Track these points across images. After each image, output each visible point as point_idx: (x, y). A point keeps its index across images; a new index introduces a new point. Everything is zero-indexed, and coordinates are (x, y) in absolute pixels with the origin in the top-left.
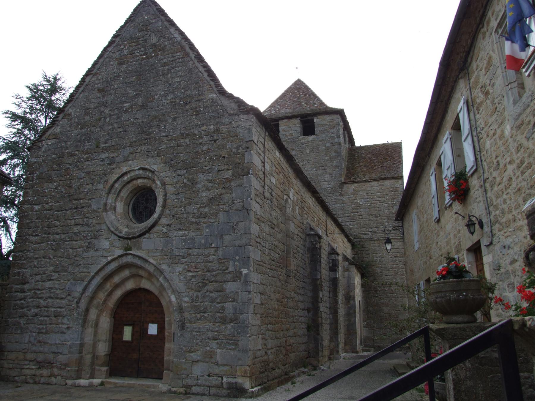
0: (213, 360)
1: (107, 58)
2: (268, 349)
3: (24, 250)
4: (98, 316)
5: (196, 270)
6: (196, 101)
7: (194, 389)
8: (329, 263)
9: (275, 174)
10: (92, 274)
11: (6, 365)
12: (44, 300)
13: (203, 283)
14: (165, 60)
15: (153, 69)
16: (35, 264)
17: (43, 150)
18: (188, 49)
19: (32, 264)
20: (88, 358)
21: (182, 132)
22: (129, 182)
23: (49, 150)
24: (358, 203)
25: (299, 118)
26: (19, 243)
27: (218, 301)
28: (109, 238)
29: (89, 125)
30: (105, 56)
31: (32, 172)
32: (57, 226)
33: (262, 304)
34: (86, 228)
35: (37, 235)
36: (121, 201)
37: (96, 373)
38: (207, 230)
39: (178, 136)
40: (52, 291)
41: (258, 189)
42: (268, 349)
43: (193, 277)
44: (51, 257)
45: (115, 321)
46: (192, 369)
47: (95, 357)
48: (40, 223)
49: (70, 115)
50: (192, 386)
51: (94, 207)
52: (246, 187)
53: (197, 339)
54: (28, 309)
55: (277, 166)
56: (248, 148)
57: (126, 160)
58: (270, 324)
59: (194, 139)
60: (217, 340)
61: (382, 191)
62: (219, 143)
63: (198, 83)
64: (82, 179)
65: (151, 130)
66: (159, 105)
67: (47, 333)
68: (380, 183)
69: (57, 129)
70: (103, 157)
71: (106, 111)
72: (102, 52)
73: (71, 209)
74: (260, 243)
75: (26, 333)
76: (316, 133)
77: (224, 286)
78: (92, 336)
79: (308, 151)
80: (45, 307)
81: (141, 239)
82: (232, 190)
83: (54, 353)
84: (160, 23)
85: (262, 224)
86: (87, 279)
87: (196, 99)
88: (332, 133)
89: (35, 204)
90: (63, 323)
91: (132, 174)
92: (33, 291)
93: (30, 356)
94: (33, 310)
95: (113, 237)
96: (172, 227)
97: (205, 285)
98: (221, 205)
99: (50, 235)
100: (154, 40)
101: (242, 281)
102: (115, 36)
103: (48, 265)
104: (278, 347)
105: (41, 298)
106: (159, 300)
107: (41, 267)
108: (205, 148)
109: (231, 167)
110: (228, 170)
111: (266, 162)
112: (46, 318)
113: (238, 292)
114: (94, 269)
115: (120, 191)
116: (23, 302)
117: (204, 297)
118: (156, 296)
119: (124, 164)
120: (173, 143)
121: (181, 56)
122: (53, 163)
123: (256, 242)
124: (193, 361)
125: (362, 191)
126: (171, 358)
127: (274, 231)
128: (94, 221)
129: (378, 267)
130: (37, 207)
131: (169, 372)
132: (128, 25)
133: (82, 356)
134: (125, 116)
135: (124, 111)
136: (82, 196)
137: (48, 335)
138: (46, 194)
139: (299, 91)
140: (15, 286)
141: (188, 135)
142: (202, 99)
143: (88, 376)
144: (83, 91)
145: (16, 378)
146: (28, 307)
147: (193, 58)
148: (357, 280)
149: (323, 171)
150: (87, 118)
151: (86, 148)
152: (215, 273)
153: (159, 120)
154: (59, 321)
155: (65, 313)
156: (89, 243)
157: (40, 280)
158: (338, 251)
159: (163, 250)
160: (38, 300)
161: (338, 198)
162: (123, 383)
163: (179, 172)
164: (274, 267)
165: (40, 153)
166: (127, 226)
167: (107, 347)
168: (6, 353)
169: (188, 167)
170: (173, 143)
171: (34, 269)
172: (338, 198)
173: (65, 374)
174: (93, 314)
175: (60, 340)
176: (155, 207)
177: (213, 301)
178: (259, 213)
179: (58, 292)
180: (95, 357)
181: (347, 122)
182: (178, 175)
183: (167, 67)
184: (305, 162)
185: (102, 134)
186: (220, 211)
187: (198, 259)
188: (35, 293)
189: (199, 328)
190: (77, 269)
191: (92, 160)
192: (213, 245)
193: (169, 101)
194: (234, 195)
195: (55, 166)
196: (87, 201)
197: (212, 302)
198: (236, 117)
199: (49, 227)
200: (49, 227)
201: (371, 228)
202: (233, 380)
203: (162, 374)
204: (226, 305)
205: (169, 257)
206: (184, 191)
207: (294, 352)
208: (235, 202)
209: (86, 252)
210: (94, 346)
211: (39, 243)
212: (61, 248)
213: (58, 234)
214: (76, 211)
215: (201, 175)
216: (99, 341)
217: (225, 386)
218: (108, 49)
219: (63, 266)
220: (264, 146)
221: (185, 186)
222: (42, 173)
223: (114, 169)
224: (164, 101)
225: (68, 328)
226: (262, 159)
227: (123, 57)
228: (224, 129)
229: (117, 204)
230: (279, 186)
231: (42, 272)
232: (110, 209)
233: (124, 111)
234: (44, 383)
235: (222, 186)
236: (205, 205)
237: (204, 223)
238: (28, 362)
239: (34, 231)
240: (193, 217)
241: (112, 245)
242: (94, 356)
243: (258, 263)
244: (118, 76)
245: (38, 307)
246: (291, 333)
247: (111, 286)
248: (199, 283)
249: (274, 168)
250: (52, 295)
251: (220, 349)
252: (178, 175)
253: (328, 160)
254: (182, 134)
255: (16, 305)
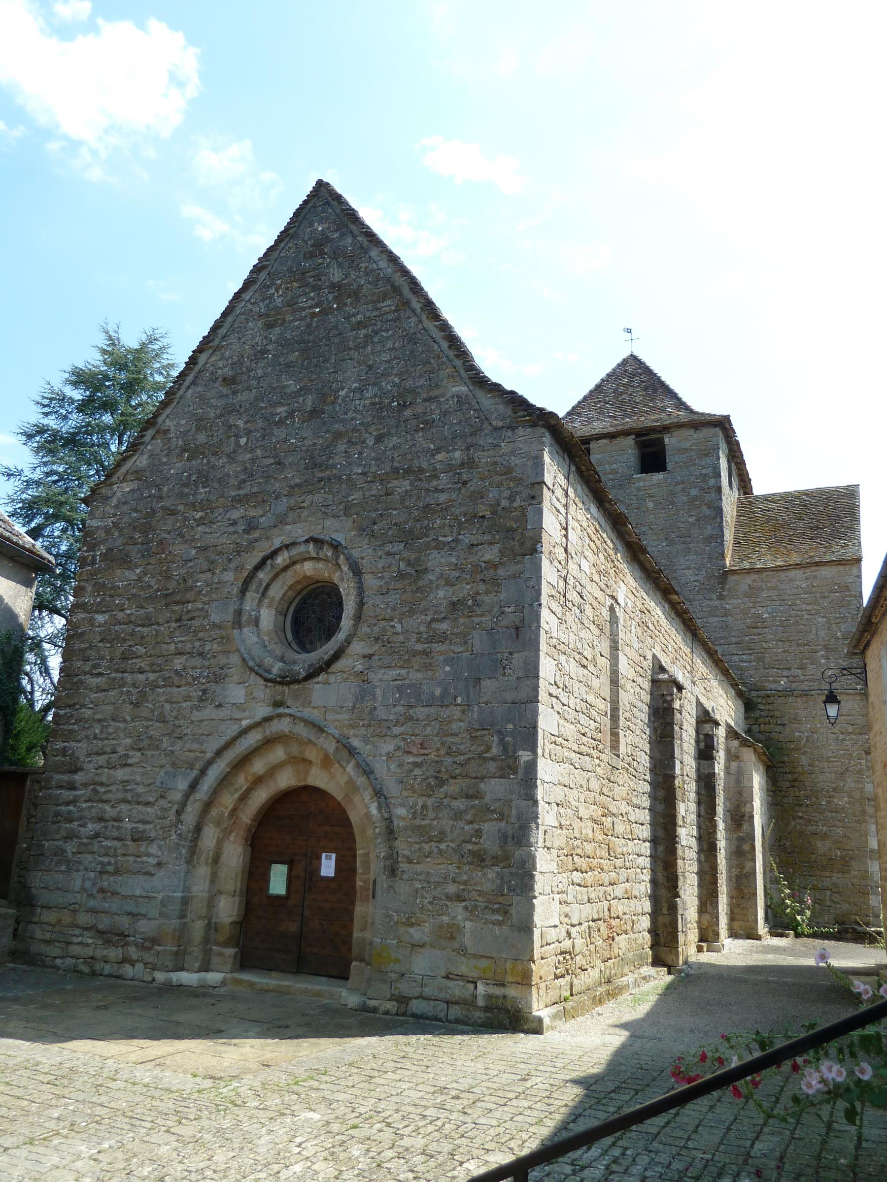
0: (456, 945)
1: (240, 314)
2: (573, 926)
3: (75, 704)
4: (220, 842)
5: (423, 751)
6: (425, 400)
7: (417, 1006)
8: (697, 741)
9: (588, 553)
10: (209, 755)
11: (38, 934)
12: (113, 807)
13: (437, 778)
14: (359, 317)
15: (335, 336)
16: (97, 731)
17: (114, 502)
18: (406, 292)
19: (90, 732)
20: (198, 928)
21: (396, 464)
22: (285, 568)
23: (125, 503)
24: (759, 616)
25: (633, 437)
26: (65, 689)
27: (469, 817)
28: (244, 682)
29: (207, 452)
30: (238, 311)
31: (92, 548)
32: (141, 656)
33: (561, 827)
34: (197, 662)
35: (100, 674)
36: (270, 606)
37: (215, 960)
38: (447, 669)
39: (387, 473)
40: (129, 788)
41: (555, 584)
42: (573, 926)
43: (417, 765)
44: (128, 718)
45: (253, 853)
46: (411, 963)
47: (211, 927)
48: (107, 650)
49: (166, 432)
50: (410, 999)
51: (215, 618)
52: (528, 579)
53: (423, 897)
54: (81, 822)
55: (593, 537)
56: (533, 498)
57: (281, 522)
58: (577, 870)
59: (421, 480)
60: (464, 900)
61: (814, 589)
62: (472, 486)
63: (428, 362)
64: (191, 560)
65: (331, 461)
66: (348, 410)
67: (117, 872)
68: (809, 572)
69: (141, 461)
70: (234, 517)
71: (240, 423)
72: (231, 302)
73: (168, 622)
74: (557, 698)
75: (78, 871)
76: (670, 466)
77: (482, 786)
78: (208, 882)
79: (651, 505)
80: (115, 820)
81: (309, 685)
82: (499, 585)
83: (129, 914)
84: (350, 240)
85: (563, 658)
86: (198, 766)
87: (424, 395)
88: (703, 467)
89: (97, 612)
90: (148, 855)
91: (294, 551)
92: (91, 787)
93: (83, 919)
94: (90, 826)
95: (253, 679)
96: (375, 661)
97: (442, 783)
98: (477, 616)
99: (126, 675)
100: (336, 275)
101: (520, 776)
102: (257, 269)
103: (122, 735)
104: (593, 921)
105: (106, 802)
106: (344, 811)
107: (107, 739)
108: (443, 497)
109: (497, 537)
110: (491, 544)
111: (569, 528)
112: (116, 843)
113: (511, 801)
114: (213, 745)
115: (268, 586)
116: (71, 808)
117: (438, 808)
118: (339, 804)
119: (275, 531)
120: (376, 489)
121: (393, 308)
122: (135, 528)
123: (550, 695)
124: (413, 945)
125: (769, 589)
126: (368, 935)
127: (586, 671)
128: (215, 646)
129: (804, 753)
130: (100, 618)
131: (363, 965)
132: (282, 244)
133: (185, 923)
134: (280, 433)
135: (276, 424)
136: (190, 596)
137: (120, 878)
138: (120, 591)
139: (634, 380)
140: (58, 777)
141: (408, 471)
142: (436, 397)
143: (197, 965)
144: (193, 383)
145: (58, 961)
146: (81, 818)
147: (418, 311)
148: (757, 781)
149: (684, 546)
150: (202, 438)
151: (199, 497)
152: (462, 758)
153: (349, 441)
154: (142, 849)
155: (153, 835)
156: (204, 692)
157: (105, 765)
158: (718, 717)
159: (354, 707)
160: (100, 805)
161: (715, 603)
162: (267, 984)
163: (388, 548)
164: (584, 749)
165: (108, 509)
166: (282, 659)
167: (236, 906)
168: (39, 910)
169: (408, 537)
170: (376, 489)
171: (95, 741)
172: (715, 603)
173: (150, 960)
174: (210, 837)
175: (143, 888)
176: (339, 618)
177: (458, 815)
178: (555, 635)
179: (140, 789)
180: (211, 927)
181: (737, 443)
182: (388, 554)
183: (363, 332)
184: (643, 529)
185: (233, 469)
186: (474, 628)
187: (428, 729)
188: (95, 791)
189: (428, 874)
190: (180, 743)
191: (211, 522)
192: (459, 700)
193: (367, 402)
194: (502, 596)
195: (137, 535)
196: (200, 605)
197: (455, 820)
198: (509, 433)
199: (125, 657)
200: (125, 657)
201: (790, 669)
202: (499, 991)
203: (348, 967)
204: (485, 827)
205: (366, 722)
206: (400, 586)
207: (626, 932)
208: (507, 610)
209: (198, 708)
210: (211, 904)
211: (104, 690)
212: (147, 701)
213: (141, 671)
214: (180, 627)
215: (435, 554)
216: (220, 892)
217: (481, 1002)
218: (243, 296)
219: (150, 738)
220: (567, 495)
221: (402, 576)
222: (112, 550)
223: (256, 540)
224: (358, 402)
225: (159, 865)
226: (563, 521)
227: (272, 313)
228: (483, 458)
229: (262, 612)
230: (596, 578)
231: (109, 749)
232: (249, 622)
233: (276, 424)
234: (110, 976)
235: (479, 577)
236: (442, 615)
237: (441, 653)
238: (81, 931)
239: (94, 667)
240: (418, 640)
241: (250, 695)
242: (209, 923)
243: (553, 738)
244: (264, 352)
245: (101, 819)
246: (619, 891)
247: (246, 779)
248: (427, 778)
249: (587, 539)
250: (129, 796)
251: (470, 920)
252: (388, 554)
253: (694, 525)
254: (396, 470)
255: (57, 814)
